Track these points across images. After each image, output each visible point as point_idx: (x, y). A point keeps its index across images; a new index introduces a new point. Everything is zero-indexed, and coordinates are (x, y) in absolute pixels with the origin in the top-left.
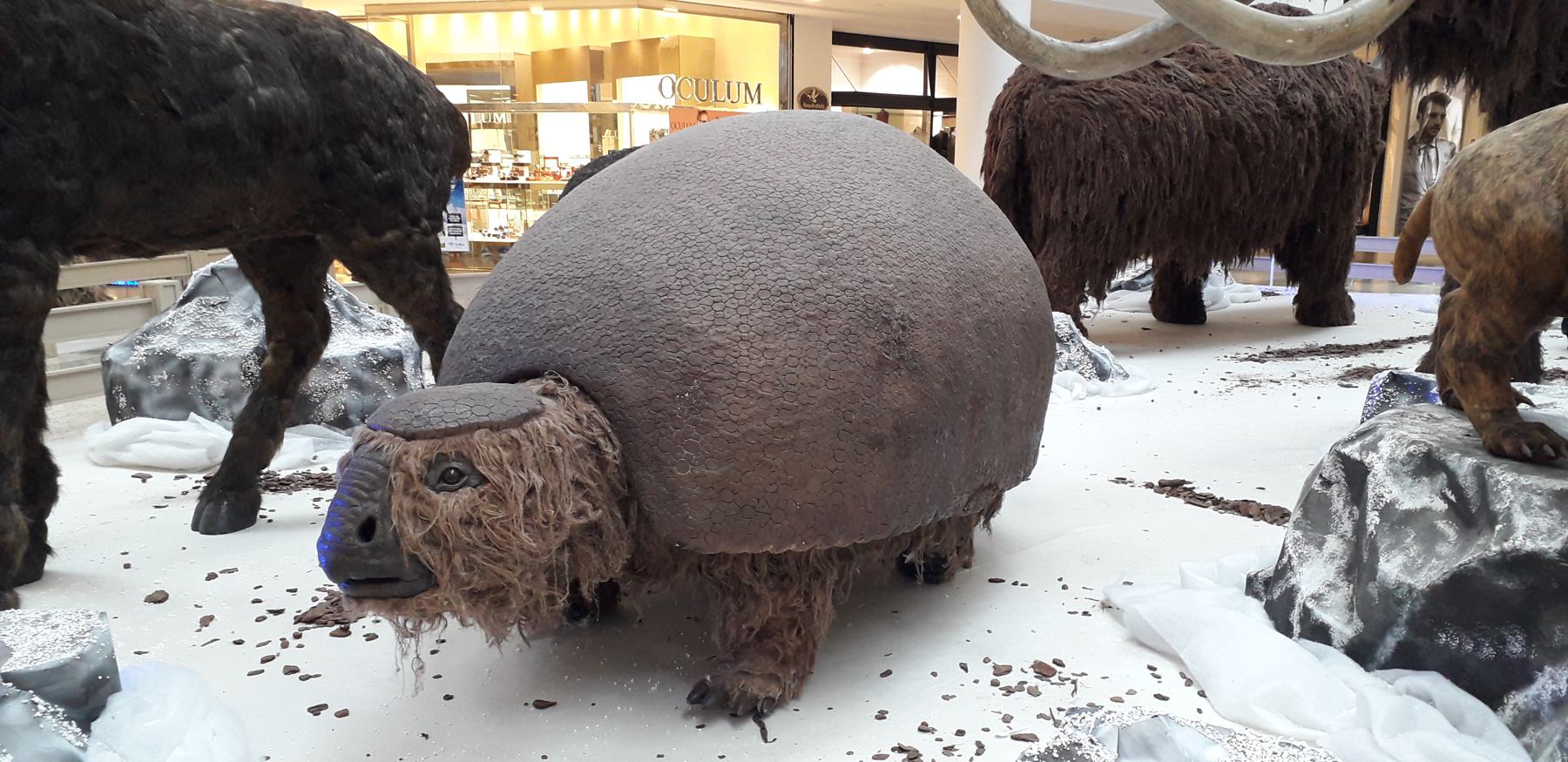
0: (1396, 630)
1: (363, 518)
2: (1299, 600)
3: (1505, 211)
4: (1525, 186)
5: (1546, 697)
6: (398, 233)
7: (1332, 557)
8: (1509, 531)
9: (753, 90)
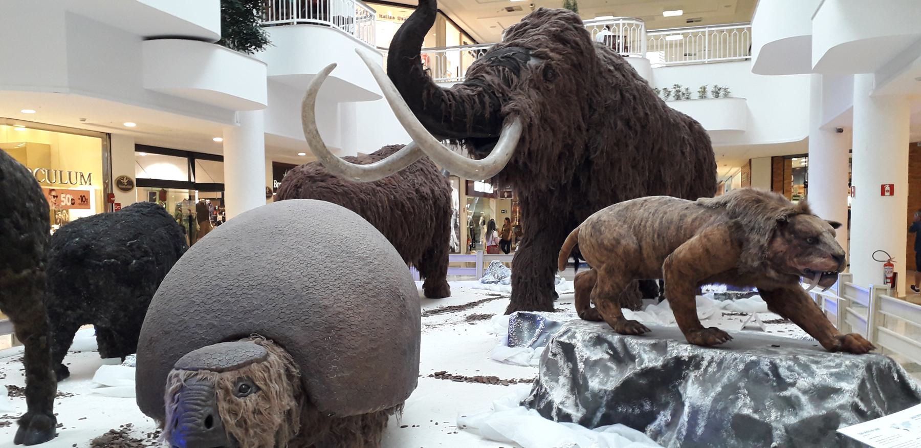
0: (601, 409)
1: (206, 416)
2: (555, 406)
3: (618, 241)
4: (623, 232)
5: (663, 423)
6: (29, 271)
7: (564, 385)
8: (642, 361)
9: (86, 177)
